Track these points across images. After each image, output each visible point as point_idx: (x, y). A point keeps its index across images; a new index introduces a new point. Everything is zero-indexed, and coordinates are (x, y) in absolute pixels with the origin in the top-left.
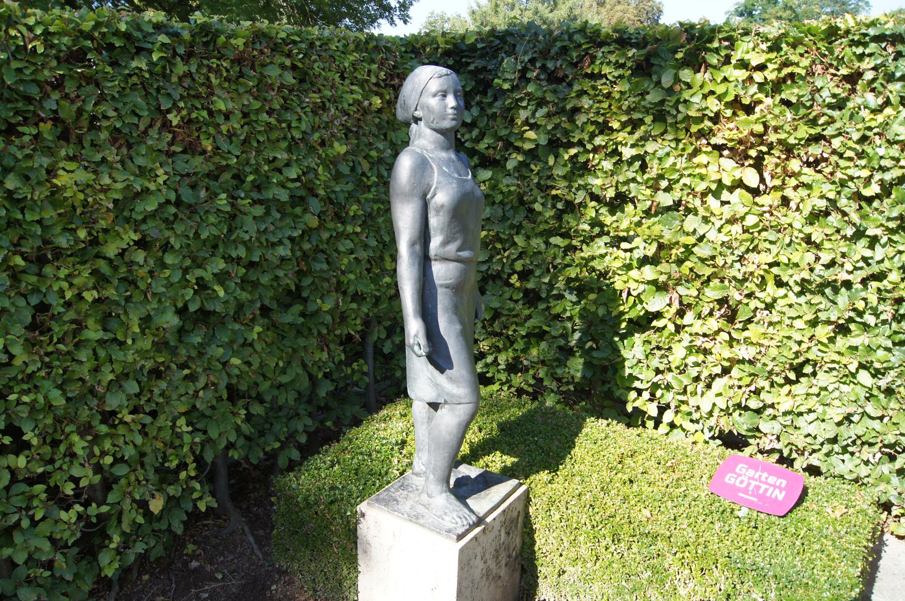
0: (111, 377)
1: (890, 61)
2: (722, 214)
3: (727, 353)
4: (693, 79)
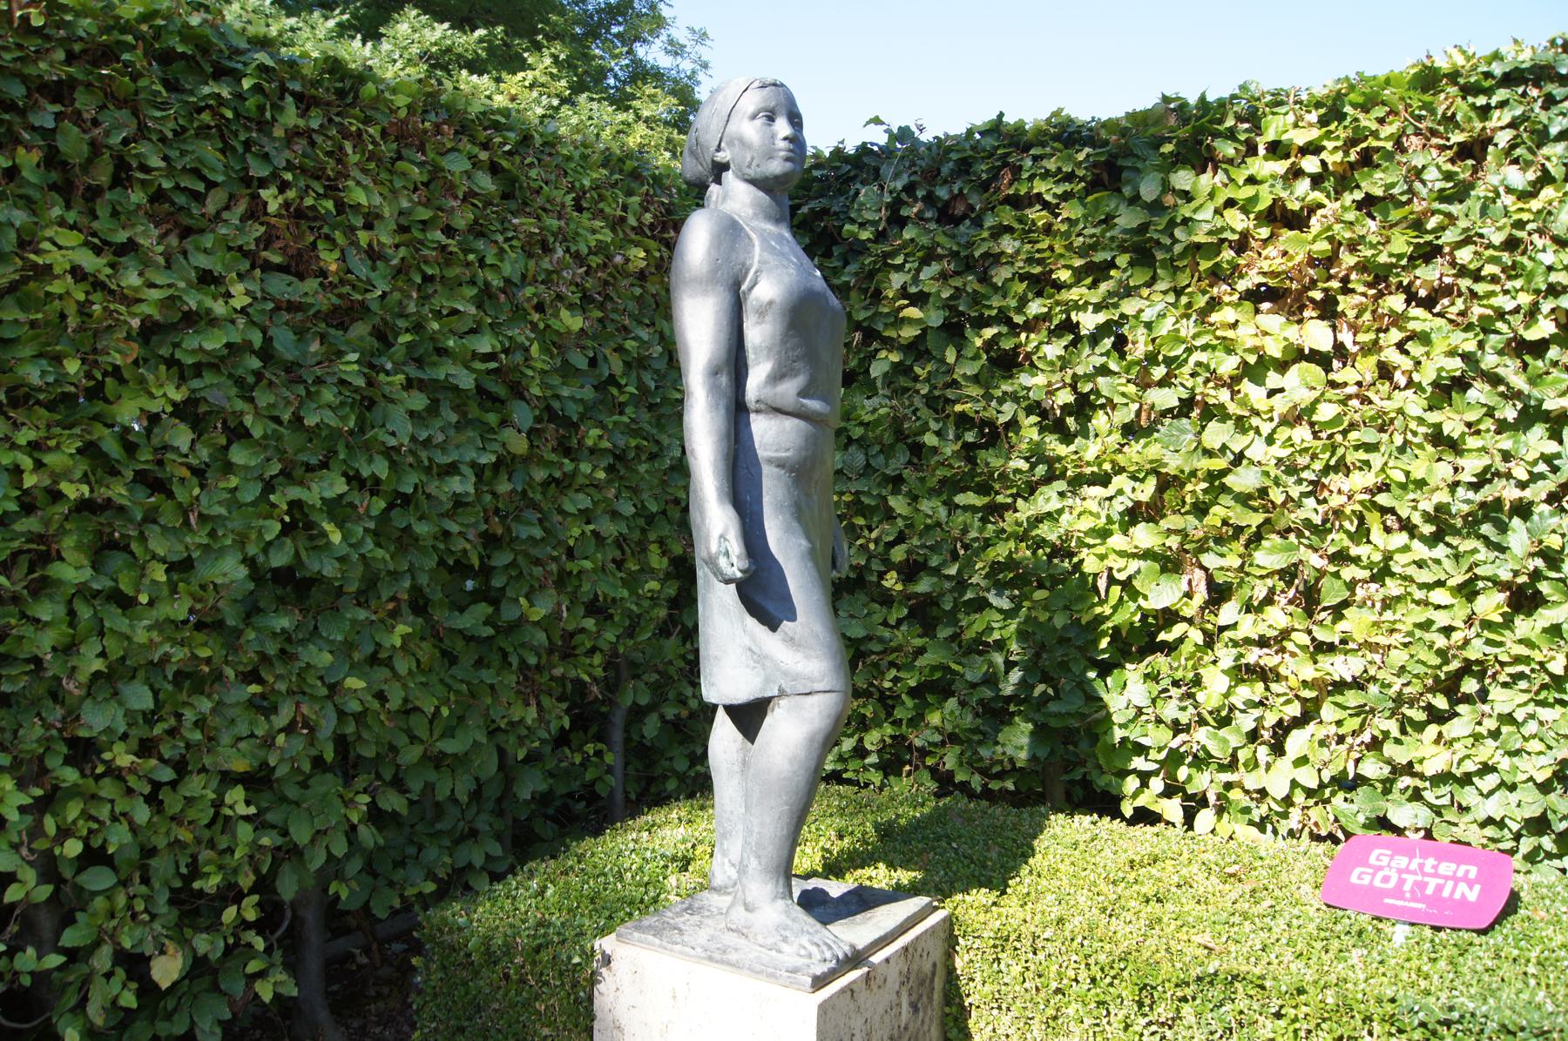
0: (98, 665)
1: (1537, 110)
2: (1271, 410)
3: (1308, 672)
4: (1195, 183)
